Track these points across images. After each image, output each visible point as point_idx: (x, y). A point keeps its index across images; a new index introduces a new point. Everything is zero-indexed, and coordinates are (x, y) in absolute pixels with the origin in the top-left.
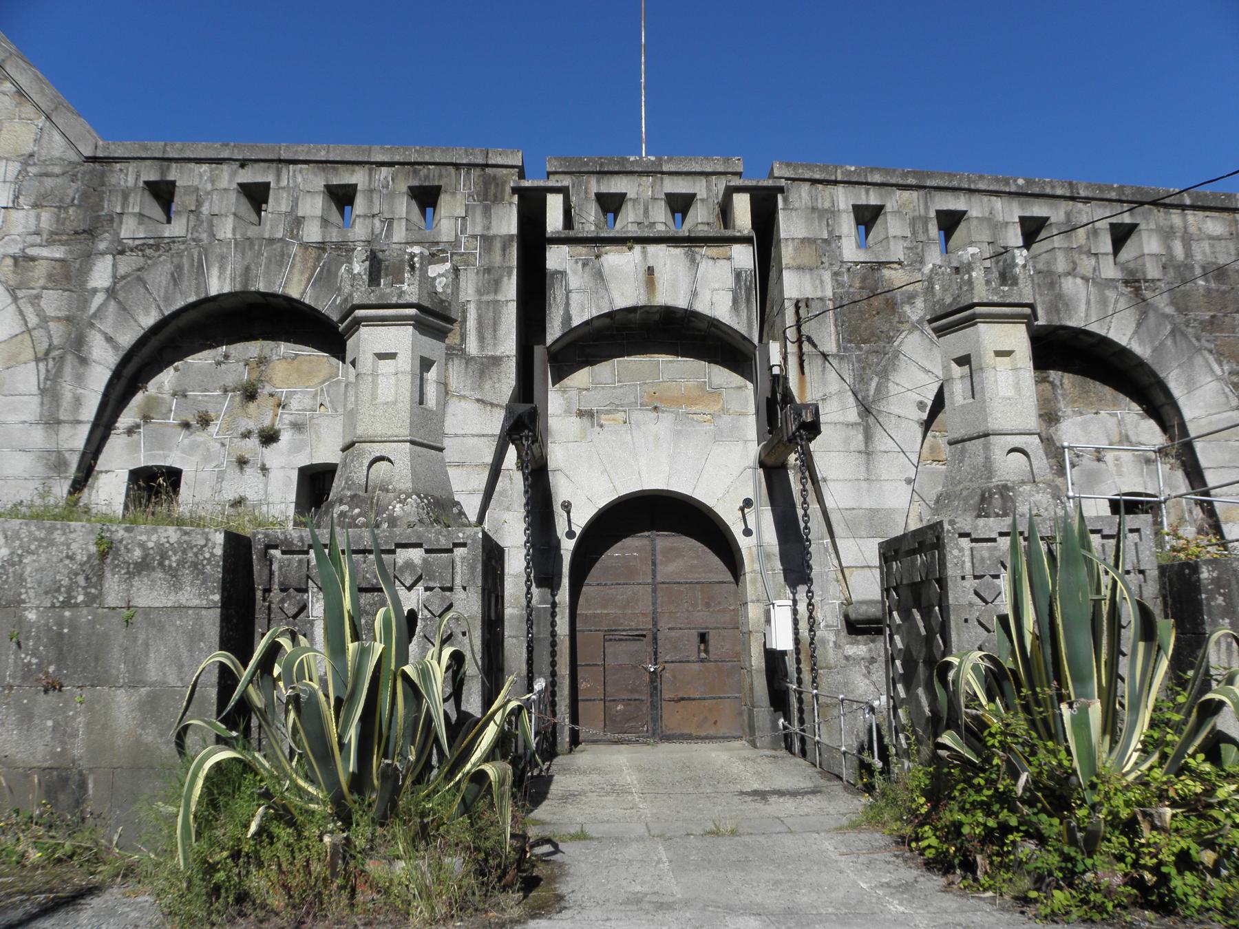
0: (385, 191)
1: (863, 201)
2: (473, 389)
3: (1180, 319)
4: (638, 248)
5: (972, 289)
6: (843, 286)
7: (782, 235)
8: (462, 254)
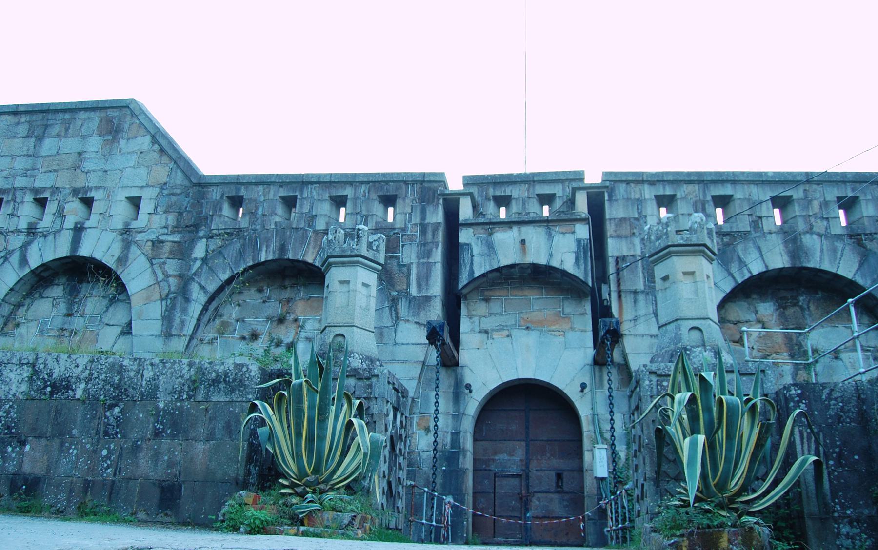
1: (661, 192)
2: (413, 316)
4: (515, 229)
7: (607, 217)
8: (409, 235)
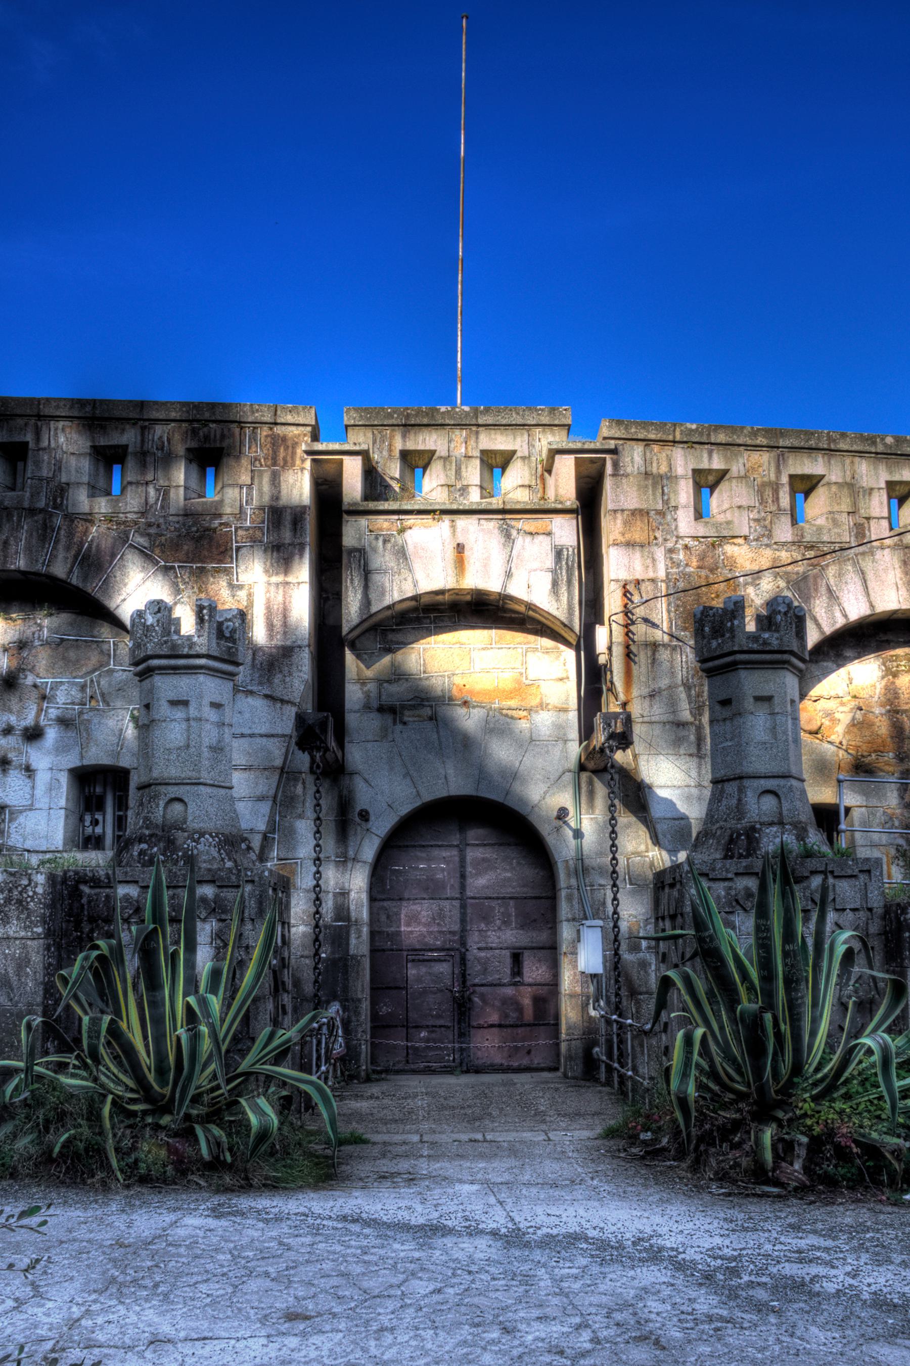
0: (159, 454)
1: (705, 465)
4: (447, 518)
5: (734, 637)
6: (678, 566)
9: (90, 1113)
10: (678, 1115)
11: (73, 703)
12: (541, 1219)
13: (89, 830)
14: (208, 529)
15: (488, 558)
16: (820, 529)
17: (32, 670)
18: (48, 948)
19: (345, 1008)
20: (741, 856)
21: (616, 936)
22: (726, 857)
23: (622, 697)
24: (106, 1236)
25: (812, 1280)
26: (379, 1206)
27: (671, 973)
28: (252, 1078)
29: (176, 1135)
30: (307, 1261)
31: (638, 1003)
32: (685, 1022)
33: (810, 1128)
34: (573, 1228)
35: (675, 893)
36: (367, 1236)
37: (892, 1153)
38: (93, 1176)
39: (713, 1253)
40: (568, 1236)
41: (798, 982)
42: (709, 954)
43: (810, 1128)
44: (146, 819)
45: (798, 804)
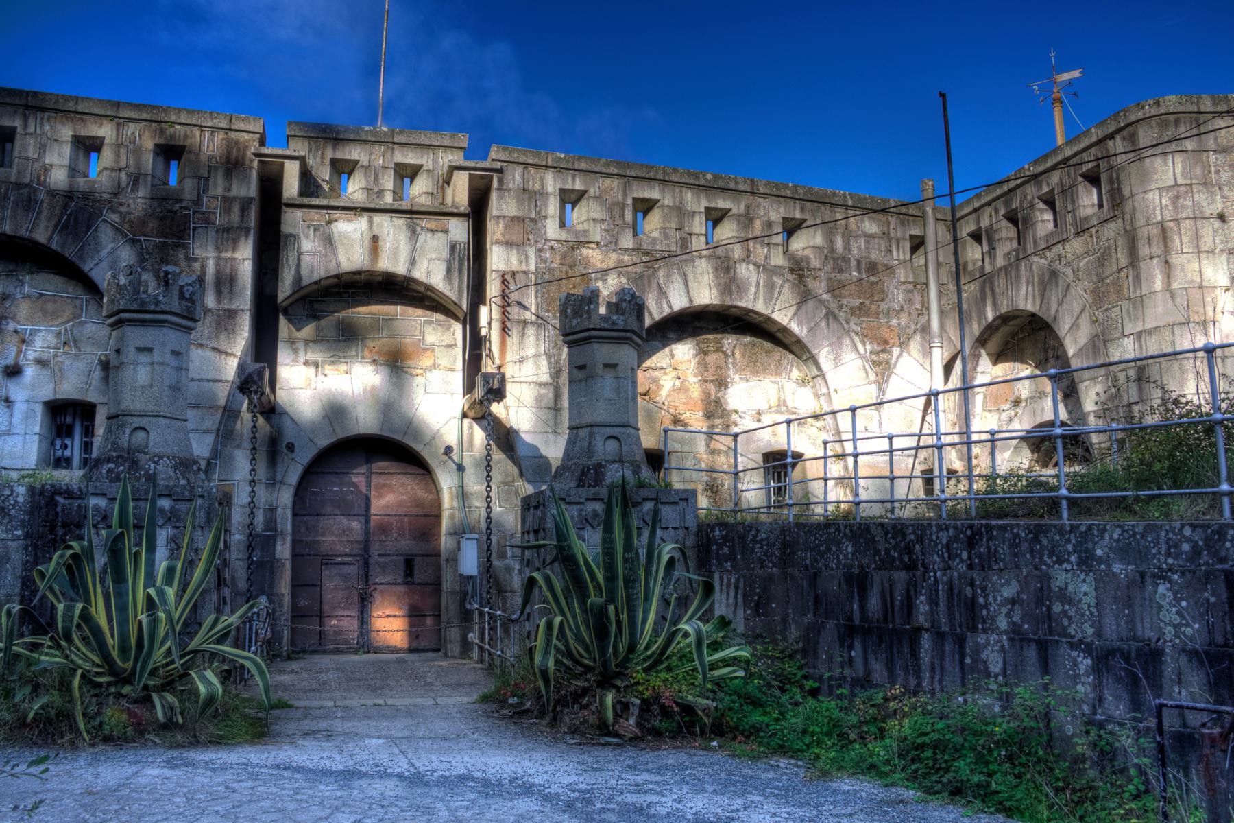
0: (131, 146)
1: (569, 186)
3: (833, 306)
4: (366, 216)
6: (546, 262)
8: (203, 213)
9: (62, 684)
10: (540, 683)
11: (49, 347)
12: (436, 764)
13: (59, 453)
14: (171, 211)
15: (397, 248)
16: (654, 239)
17: (14, 318)
18: (26, 548)
19: (271, 601)
20: (590, 486)
21: (489, 547)
22: (578, 486)
23: (498, 362)
24: (77, 787)
25: (648, 806)
26: (305, 757)
27: (534, 574)
28: (199, 655)
29: (135, 701)
30: (250, 801)
31: (504, 599)
32: (546, 612)
33: (642, 693)
34: (461, 770)
35: (539, 513)
36: (297, 780)
37: (704, 711)
38: (62, 737)
39: (572, 787)
40: (459, 776)
41: (634, 581)
42: (566, 558)
43: (642, 693)
44: (114, 443)
45: (635, 447)
